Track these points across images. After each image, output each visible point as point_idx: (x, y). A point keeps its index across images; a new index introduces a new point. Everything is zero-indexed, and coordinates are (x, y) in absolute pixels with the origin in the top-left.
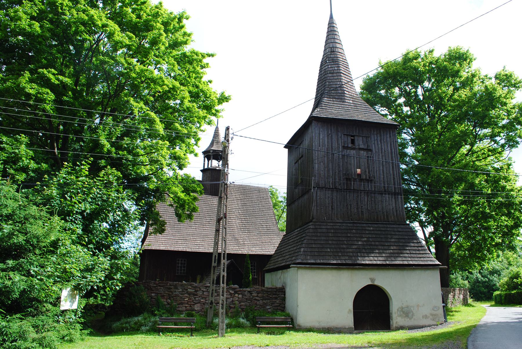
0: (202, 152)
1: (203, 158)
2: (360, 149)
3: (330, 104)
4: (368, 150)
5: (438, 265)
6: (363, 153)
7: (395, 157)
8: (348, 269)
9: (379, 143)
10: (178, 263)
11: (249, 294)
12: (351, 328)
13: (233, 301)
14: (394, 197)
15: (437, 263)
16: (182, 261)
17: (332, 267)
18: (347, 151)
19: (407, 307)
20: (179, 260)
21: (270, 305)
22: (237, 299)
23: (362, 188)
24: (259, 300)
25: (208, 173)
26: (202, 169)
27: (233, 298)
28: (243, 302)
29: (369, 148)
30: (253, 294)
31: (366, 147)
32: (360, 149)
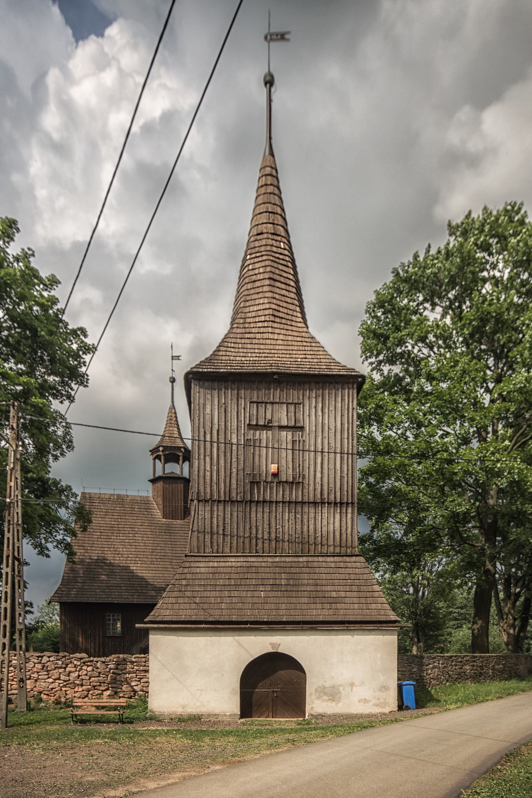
0: (150, 451)
1: (152, 461)
2: (281, 428)
3: (277, 347)
4: (298, 428)
5: (395, 622)
6: (286, 436)
7: (348, 439)
8: (160, 632)
9: (320, 413)
10: (109, 620)
11: (103, 666)
12: (235, 715)
13: (79, 676)
14: (338, 511)
15: (393, 617)
16: (113, 616)
17: (166, 628)
18: (254, 435)
19: (333, 687)
20: (109, 616)
21: (136, 681)
22: (85, 672)
23: (280, 498)
24: (120, 674)
25: (160, 484)
26: (152, 477)
27: (79, 671)
28: (94, 677)
29: (298, 425)
30: (109, 666)
31: (292, 423)
32: (281, 428)
